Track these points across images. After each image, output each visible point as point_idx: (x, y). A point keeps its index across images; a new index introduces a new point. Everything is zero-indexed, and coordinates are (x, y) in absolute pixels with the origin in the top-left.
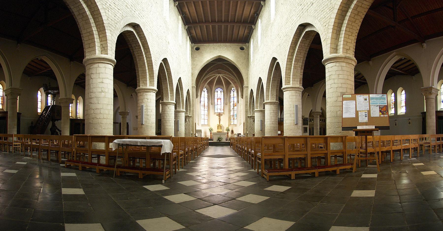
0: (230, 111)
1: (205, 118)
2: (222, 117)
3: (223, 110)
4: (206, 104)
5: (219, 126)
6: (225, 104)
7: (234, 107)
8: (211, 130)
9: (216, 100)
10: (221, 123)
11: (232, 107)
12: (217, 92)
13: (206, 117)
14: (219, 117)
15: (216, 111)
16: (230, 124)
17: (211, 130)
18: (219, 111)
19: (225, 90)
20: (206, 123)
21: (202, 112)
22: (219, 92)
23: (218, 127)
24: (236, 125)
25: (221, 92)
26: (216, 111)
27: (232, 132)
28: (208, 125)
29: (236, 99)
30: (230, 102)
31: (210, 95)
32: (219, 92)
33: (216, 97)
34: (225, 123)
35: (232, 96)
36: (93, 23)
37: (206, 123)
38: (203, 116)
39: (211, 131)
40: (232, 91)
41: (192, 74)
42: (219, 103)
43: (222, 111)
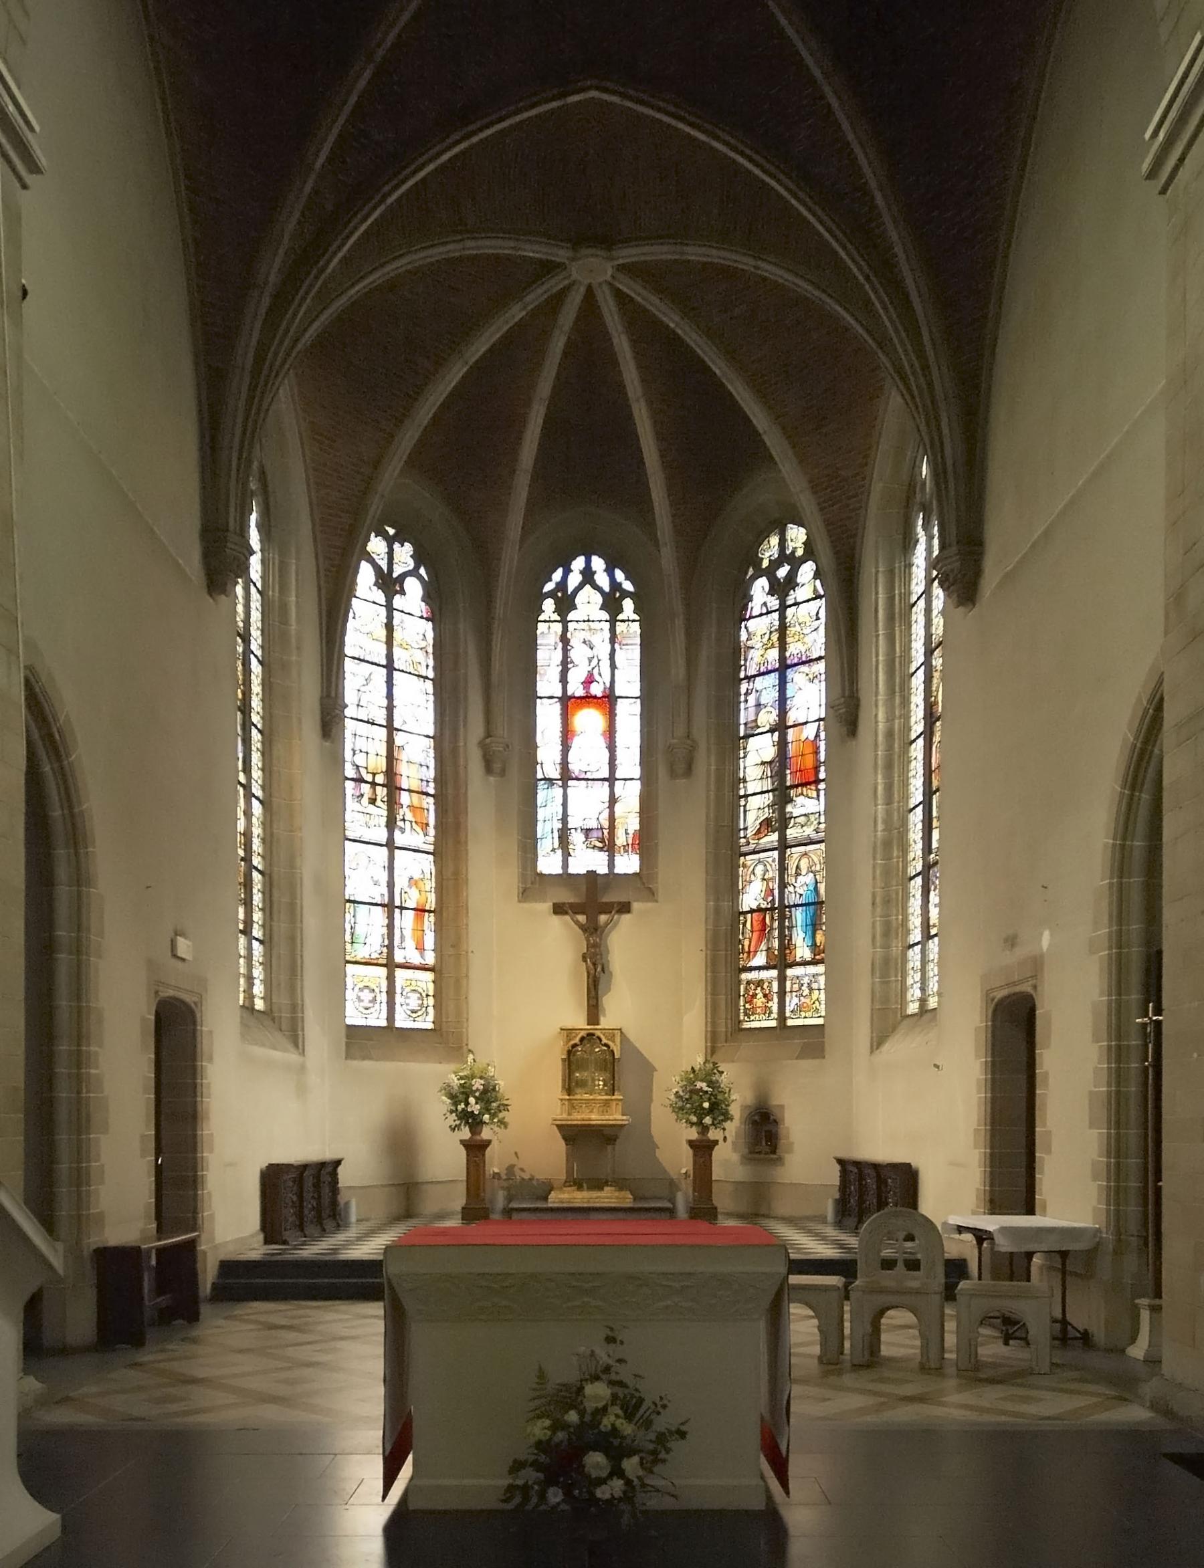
0: (726, 854)
1: (406, 952)
2: (624, 939)
3: (645, 842)
4: (418, 761)
5: (590, 1057)
6: (666, 758)
7: (782, 796)
8: (476, 1106)
9: (548, 717)
10: (621, 1011)
11: (756, 809)
12: (566, 603)
13: (417, 943)
14: (593, 931)
15: (549, 863)
16: (726, 1029)
17: (476, 1106)
18: (588, 860)
19: (668, 556)
20: (416, 1014)
21: (363, 874)
22: (589, 603)
23: (571, 1061)
24: (812, 1042)
25: (612, 604)
26: (549, 863)
27: (765, 1130)
28: (446, 1037)
29: (809, 698)
30: (731, 742)
31: (471, 650)
32: (589, 603)
33: (547, 683)
34: (658, 1008)
35: (759, 652)
36: (951, 1332)
37: (416, 1014)
38: (368, 928)
39: (473, 1121)
40: (760, 587)
41: (690, 1274)
42: (588, 753)
43: (628, 864)
